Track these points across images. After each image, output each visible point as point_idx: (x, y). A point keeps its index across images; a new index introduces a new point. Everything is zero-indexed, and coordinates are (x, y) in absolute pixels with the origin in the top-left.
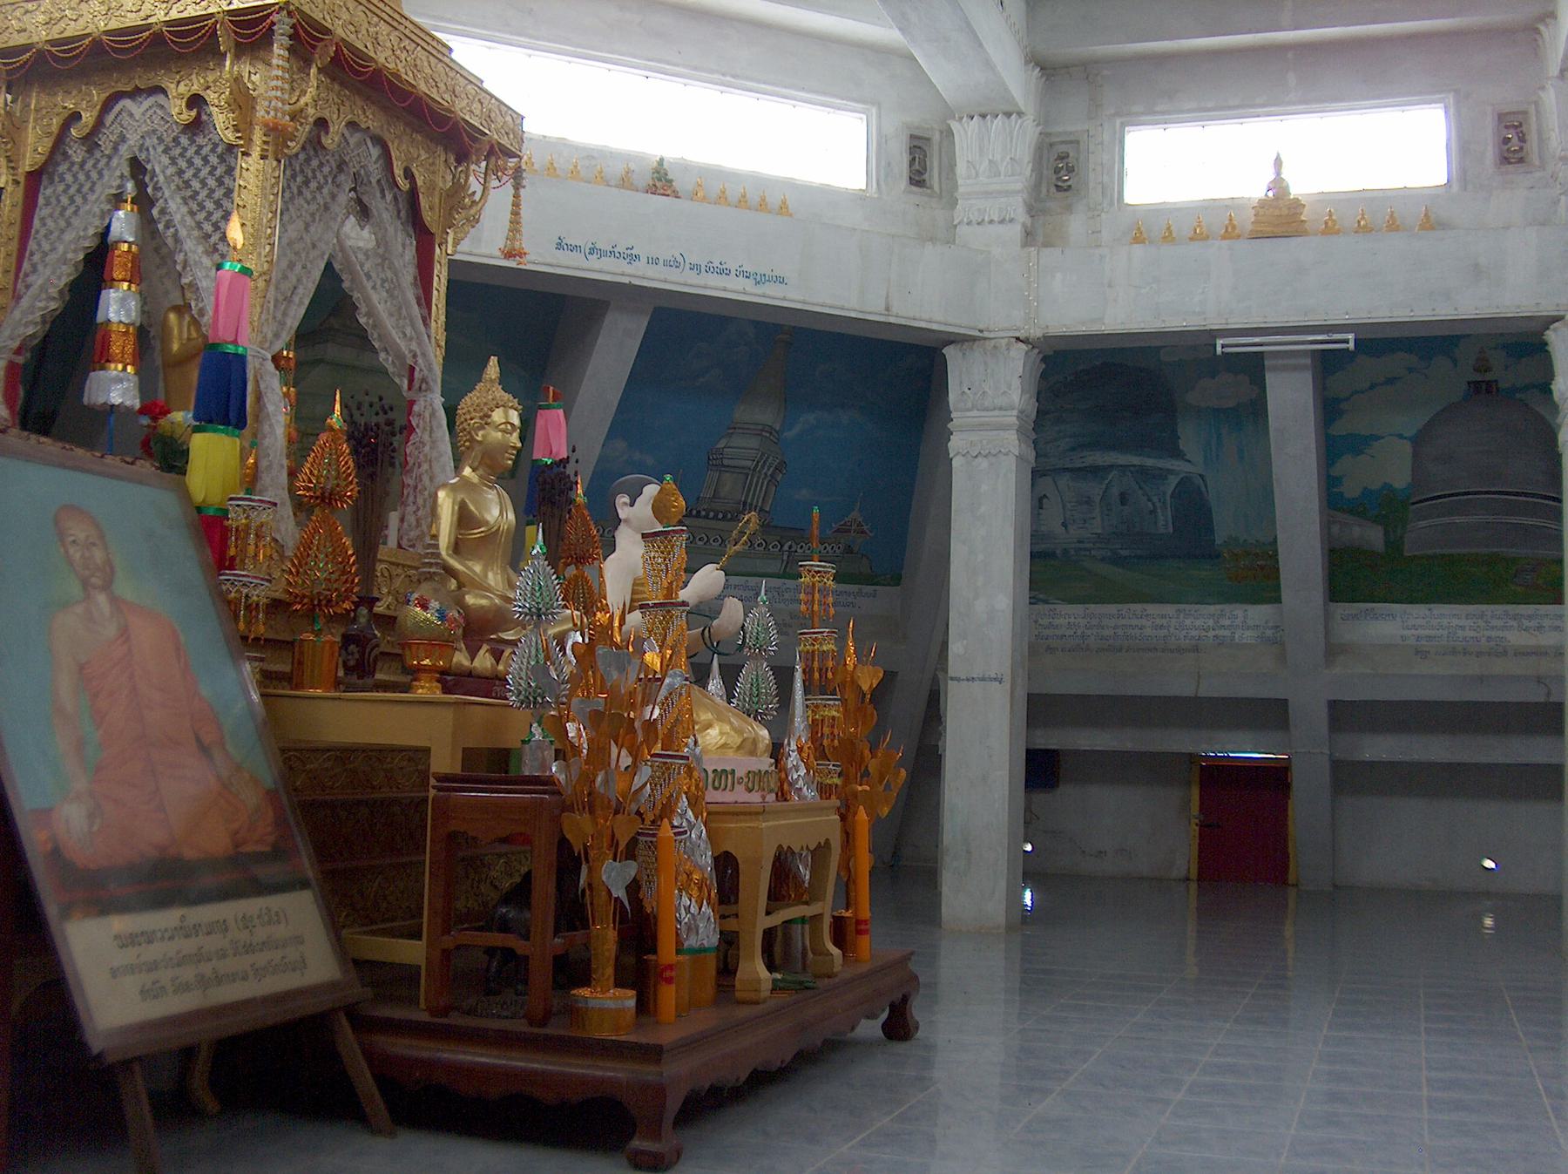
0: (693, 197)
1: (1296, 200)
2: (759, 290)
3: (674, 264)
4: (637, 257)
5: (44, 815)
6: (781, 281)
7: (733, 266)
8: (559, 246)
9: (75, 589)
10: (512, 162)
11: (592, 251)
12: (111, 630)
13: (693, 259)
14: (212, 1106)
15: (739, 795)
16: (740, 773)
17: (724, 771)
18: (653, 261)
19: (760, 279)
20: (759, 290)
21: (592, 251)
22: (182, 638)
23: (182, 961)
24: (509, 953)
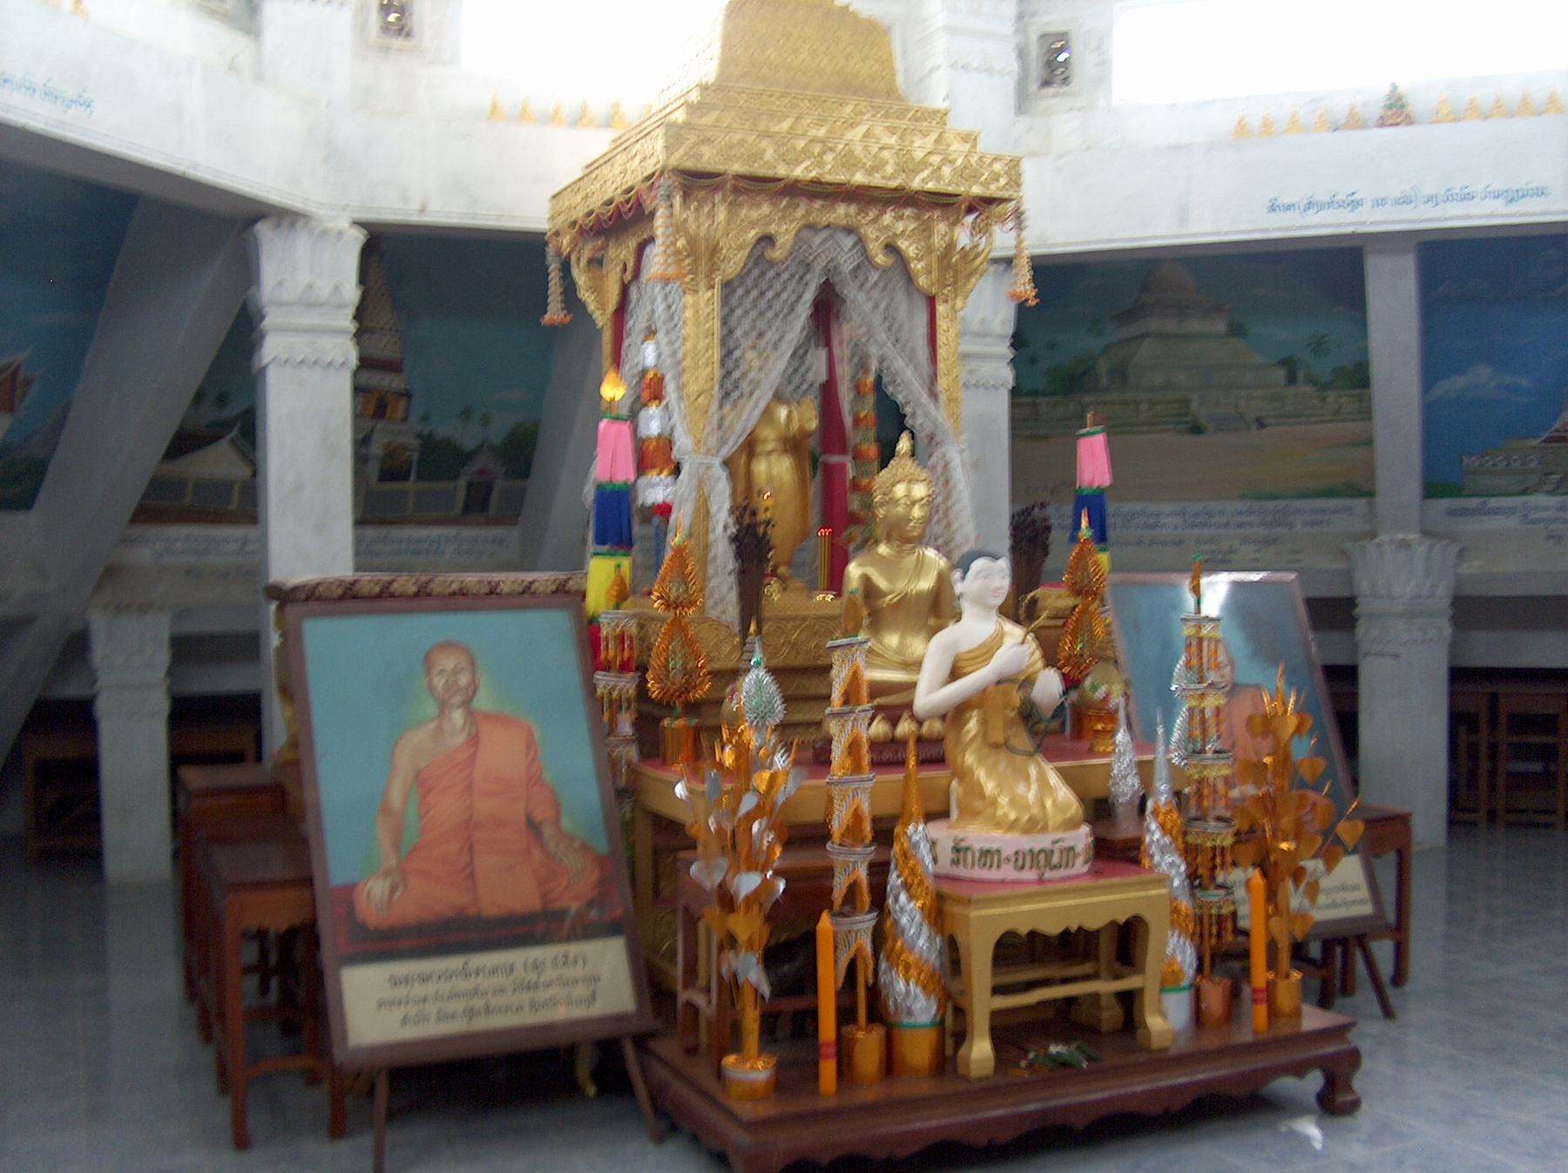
0: (1437, 118)
1: (660, 436)
2: (1513, 208)
3: (1405, 200)
4: (1359, 203)
5: (349, 891)
6: (1540, 192)
7: (1477, 187)
8: (1272, 208)
9: (432, 709)
10: (1011, 205)
11: (1310, 205)
12: (460, 739)
13: (1427, 191)
14: (591, 1090)
15: (1008, 872)
16: (1008, 851)
17: (988, 851)
18: (1380, 202)
19: (1513, 196)
20: (1513, 208)
21: (1310, 205)
22: (537, 735)
23: (453, 996)
24: (1212, 957)
